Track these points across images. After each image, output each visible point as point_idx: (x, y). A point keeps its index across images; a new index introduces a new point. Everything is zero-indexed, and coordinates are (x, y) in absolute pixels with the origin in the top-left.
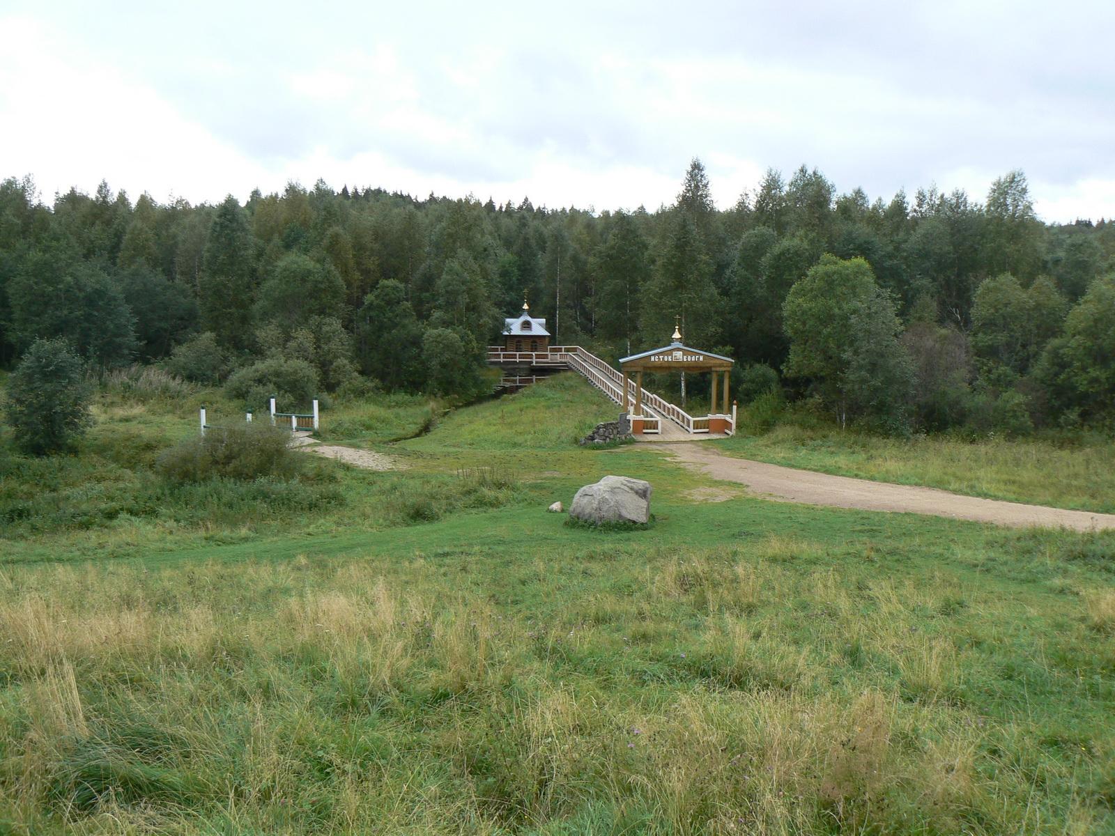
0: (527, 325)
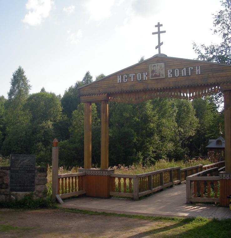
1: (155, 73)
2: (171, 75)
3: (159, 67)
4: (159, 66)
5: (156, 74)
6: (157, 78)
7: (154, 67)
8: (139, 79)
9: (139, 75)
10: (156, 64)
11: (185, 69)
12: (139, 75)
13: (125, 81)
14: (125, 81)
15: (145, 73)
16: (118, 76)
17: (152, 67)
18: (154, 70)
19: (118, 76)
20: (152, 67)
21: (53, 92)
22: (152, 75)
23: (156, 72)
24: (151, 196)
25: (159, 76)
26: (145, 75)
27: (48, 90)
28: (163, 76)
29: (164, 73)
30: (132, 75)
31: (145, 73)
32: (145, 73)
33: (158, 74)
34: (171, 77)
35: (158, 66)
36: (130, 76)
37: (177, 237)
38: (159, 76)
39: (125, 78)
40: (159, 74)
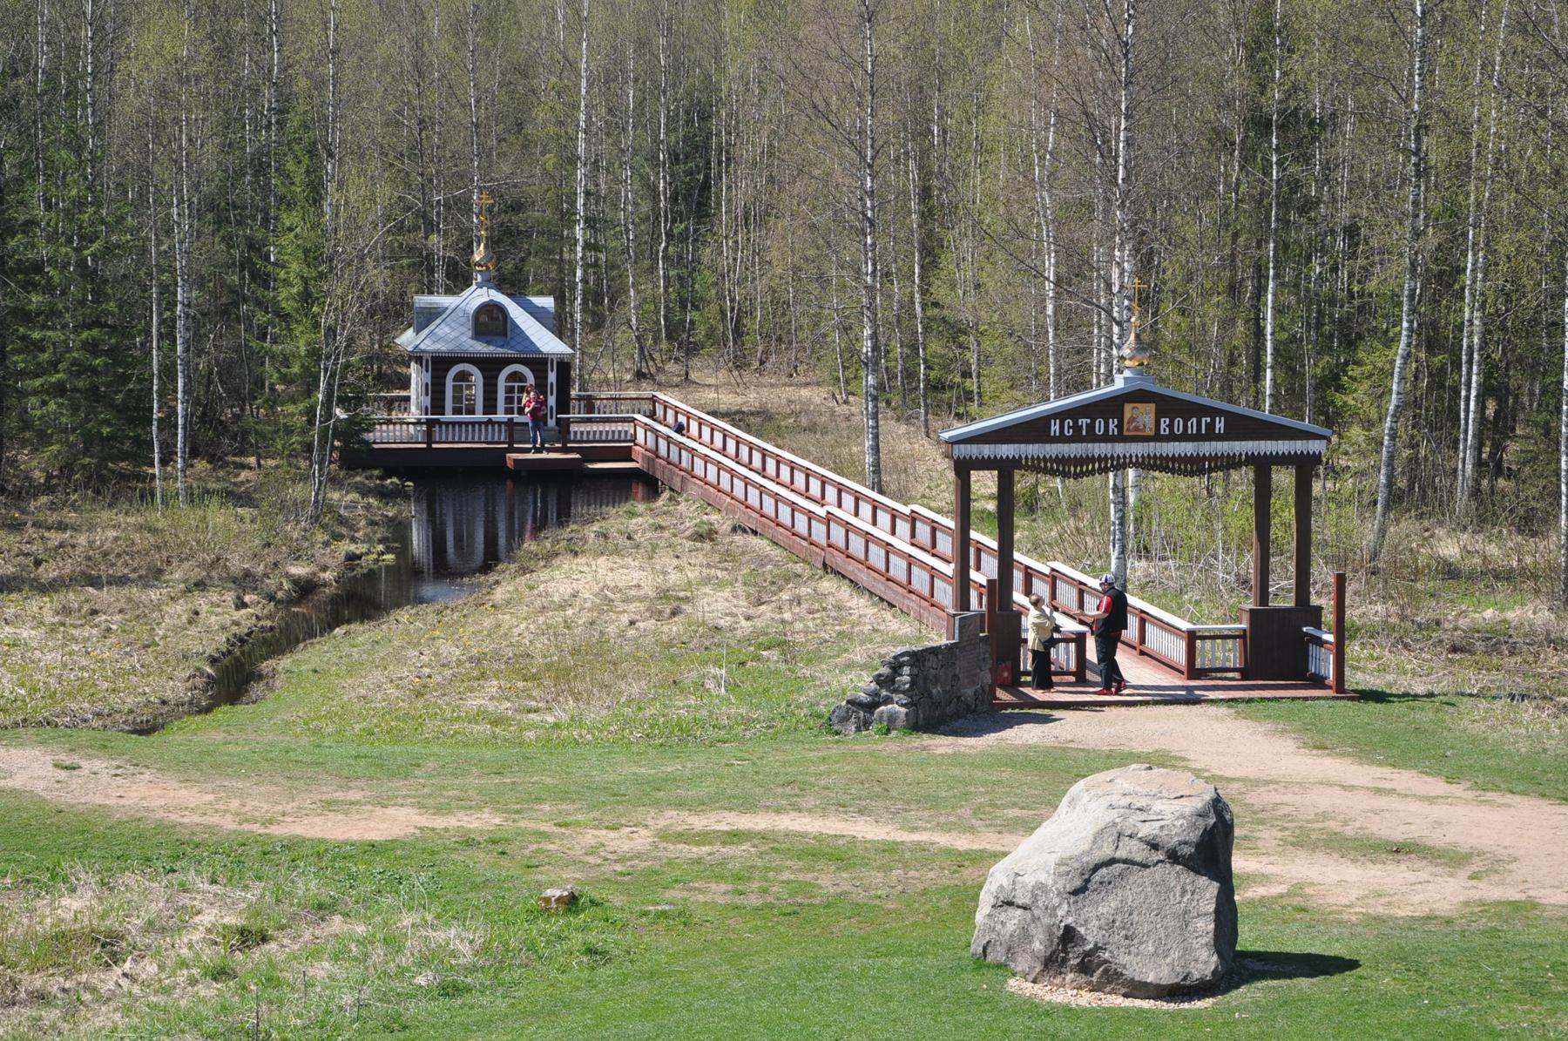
39: (1069, 427)
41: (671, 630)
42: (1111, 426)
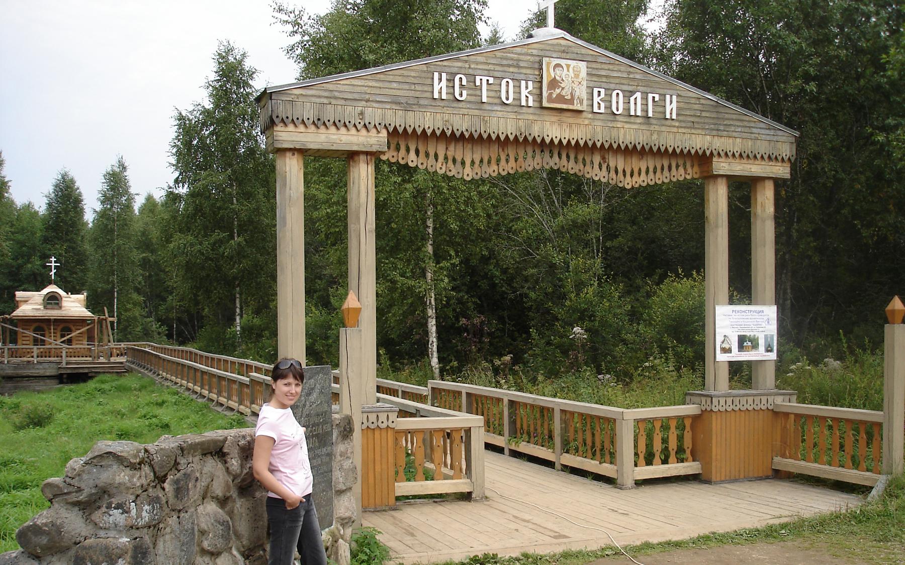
0: (53, 300)
1: (558, 91)
2: (603, 105)
3: (571, 74)
4: (571, 70)
5: (563, 93)
6: (564, 106)
7: (556, 70)
8: (618, 94)
9: (508, 86)
10: (563, 62)
11: (638, 95)
12: (508, 86)
13: (461, 95)
14: (461, 95)
15: (527, 84)
16: (436, 75)
17: (551, 70)
18: (558, 78)
19: (436, 75)
20: (551, 70)
21: (76, 179)
22: (551, 94)
23: (563, 89)
24: (25, 392)
25: (571, 101)
26: (527, 88)
27: (154, 195)
28: (581, 102)
29: (584, 96)
30: (485, 79)
31: (527, 84)
32: (527, 81)
33: (566, 93)
34: (602, 110)
35: (568, 71)
36: (478, 83)
37: (2, 363)
38: (571, 101)
40: (572, 94)
41: (53, 300)
42: (524, 92)
